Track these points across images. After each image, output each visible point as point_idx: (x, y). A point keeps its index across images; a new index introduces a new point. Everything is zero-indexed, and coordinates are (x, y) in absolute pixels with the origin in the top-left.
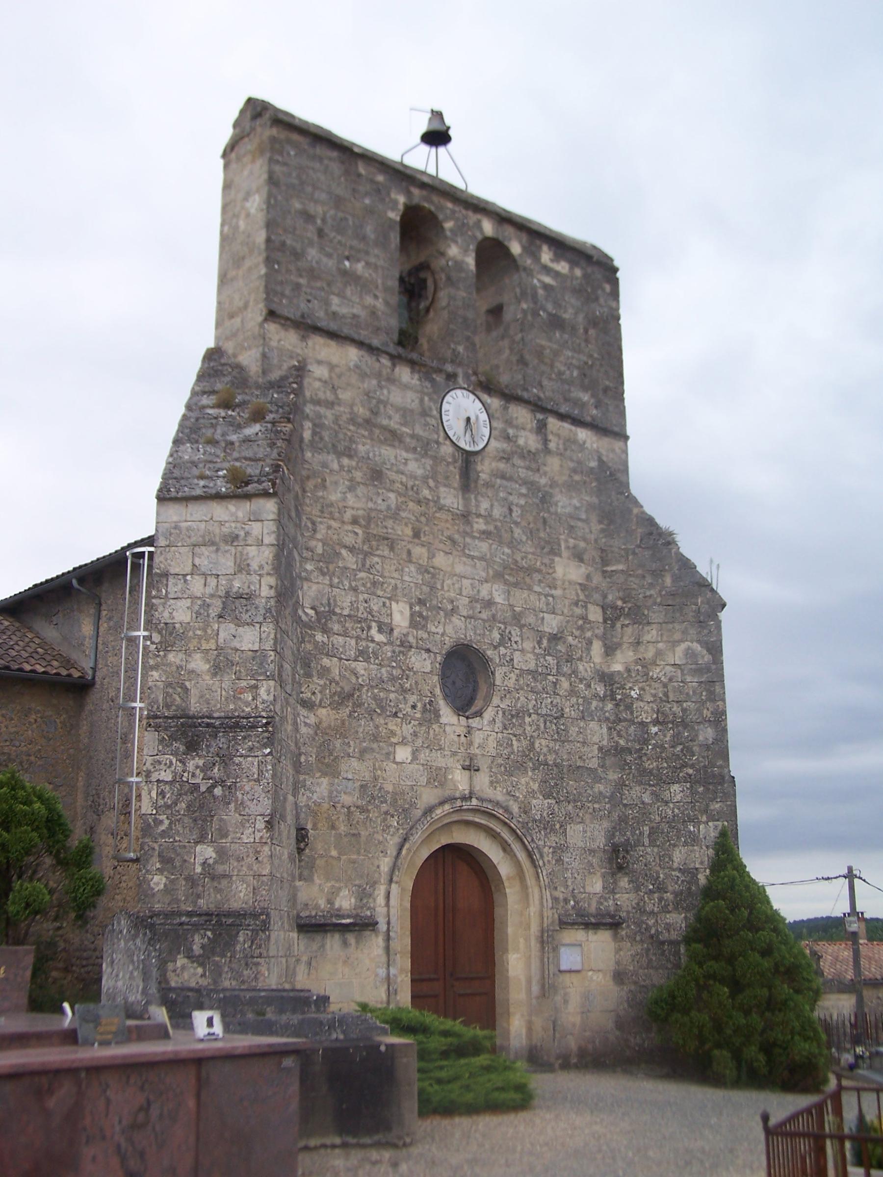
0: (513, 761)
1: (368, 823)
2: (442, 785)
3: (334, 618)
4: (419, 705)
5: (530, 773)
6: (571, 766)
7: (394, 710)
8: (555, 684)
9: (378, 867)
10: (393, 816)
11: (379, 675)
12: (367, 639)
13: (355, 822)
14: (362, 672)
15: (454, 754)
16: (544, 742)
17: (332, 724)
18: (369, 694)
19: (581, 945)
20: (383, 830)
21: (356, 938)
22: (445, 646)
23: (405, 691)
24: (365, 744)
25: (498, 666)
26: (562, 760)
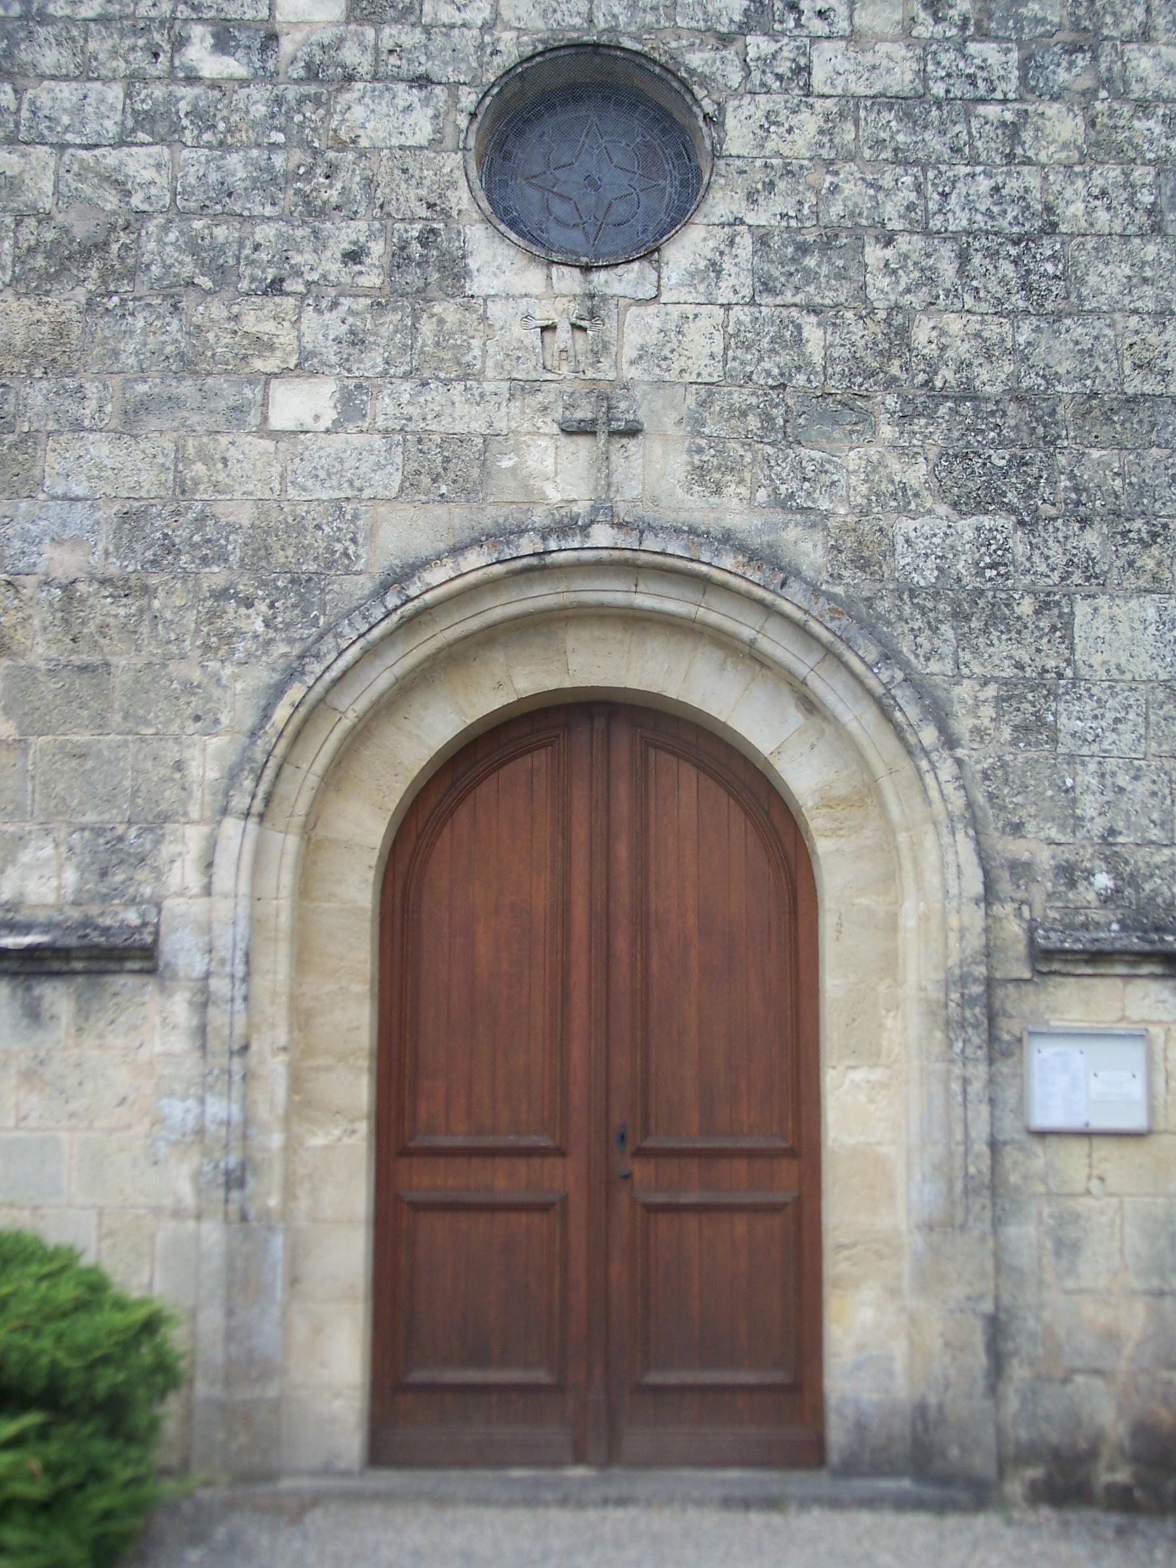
0: (804, 394)
1: (145, 629)
2: (468, 491)
3: (42, 32)
4: (377, 248)
5: (887, 431)
6: (1094, 395)
7: (271, 274)
8: (1012, 131)
9: (179, 766)
10: (248, 603)
11: (214, 177)
12: (171, 76)
13: (92, 627)
14: (148, 175)
15: (522, 388)
16: (954, 324)
17: (18, 341)
18: (172, 237)
19: (1141, 1036)
20: (206, 647)
21: (79, 997)
22: (497, 60)
23: (314, 211)
24: (142, 388)
25: (735, 93)
26: (1051, 379)
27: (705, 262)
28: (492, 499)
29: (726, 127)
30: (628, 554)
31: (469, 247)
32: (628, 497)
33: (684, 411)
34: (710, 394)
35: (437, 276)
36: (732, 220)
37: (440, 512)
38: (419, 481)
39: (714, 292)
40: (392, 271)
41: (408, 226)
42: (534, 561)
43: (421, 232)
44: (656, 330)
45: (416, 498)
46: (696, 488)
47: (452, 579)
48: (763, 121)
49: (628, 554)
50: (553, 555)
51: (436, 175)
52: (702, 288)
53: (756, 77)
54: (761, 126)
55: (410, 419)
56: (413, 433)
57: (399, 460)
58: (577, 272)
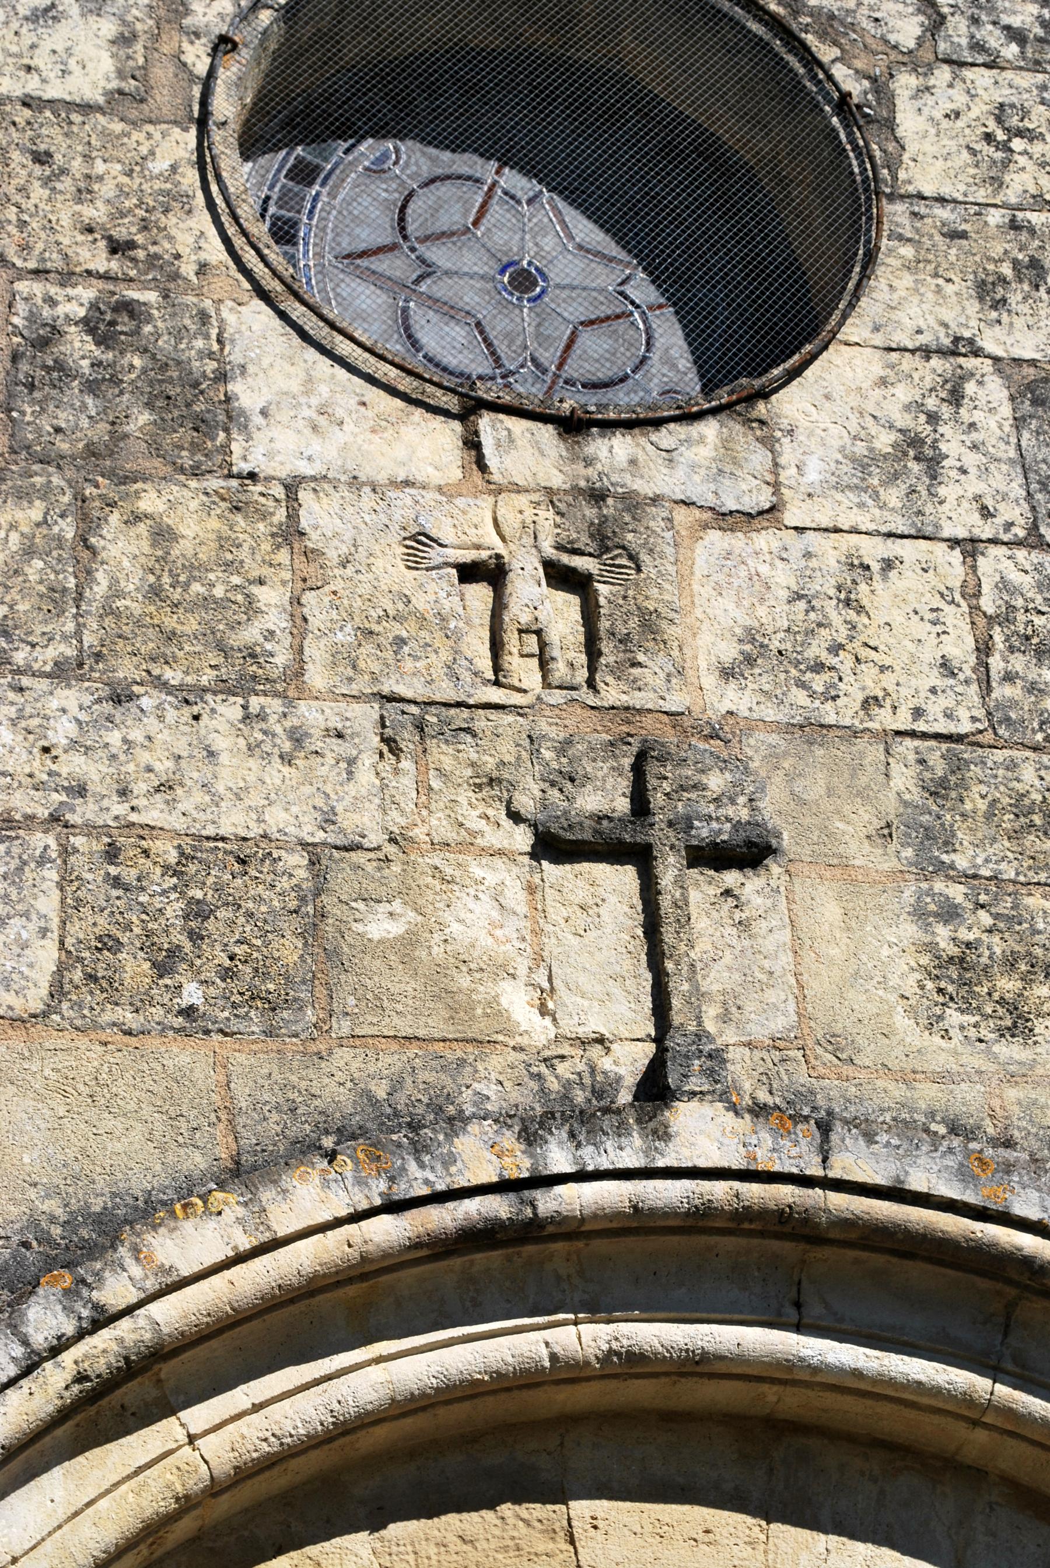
27: (893, 437)
28: (345, 1027)
29: (900, 132)
30: (786, 1193)
31: (235, 355)
32: (761, 1030)
33: (891, 806)
34: (957, 765)
35: (144, 418)
36: (947, 342)
37: (184, 1059)
38: (117, 969)
39: (929, 509)
40: (11, 395)
41: (53, 290)
42: (499, 1207)
43: (94, 306)
44: (784, 594)
45: (107, 1017)
46: (954, 1017)
47: (240, 1258)
48: (992, 125)
49: (786, 1193)
50: (559, 1189)
51: (129, 174)
52: (893, 496)
53: (958, 29)
54: (989, 137)
55: (80, 791)
56: (90, 829)
57: (48, 904)
58: (547, 433)
